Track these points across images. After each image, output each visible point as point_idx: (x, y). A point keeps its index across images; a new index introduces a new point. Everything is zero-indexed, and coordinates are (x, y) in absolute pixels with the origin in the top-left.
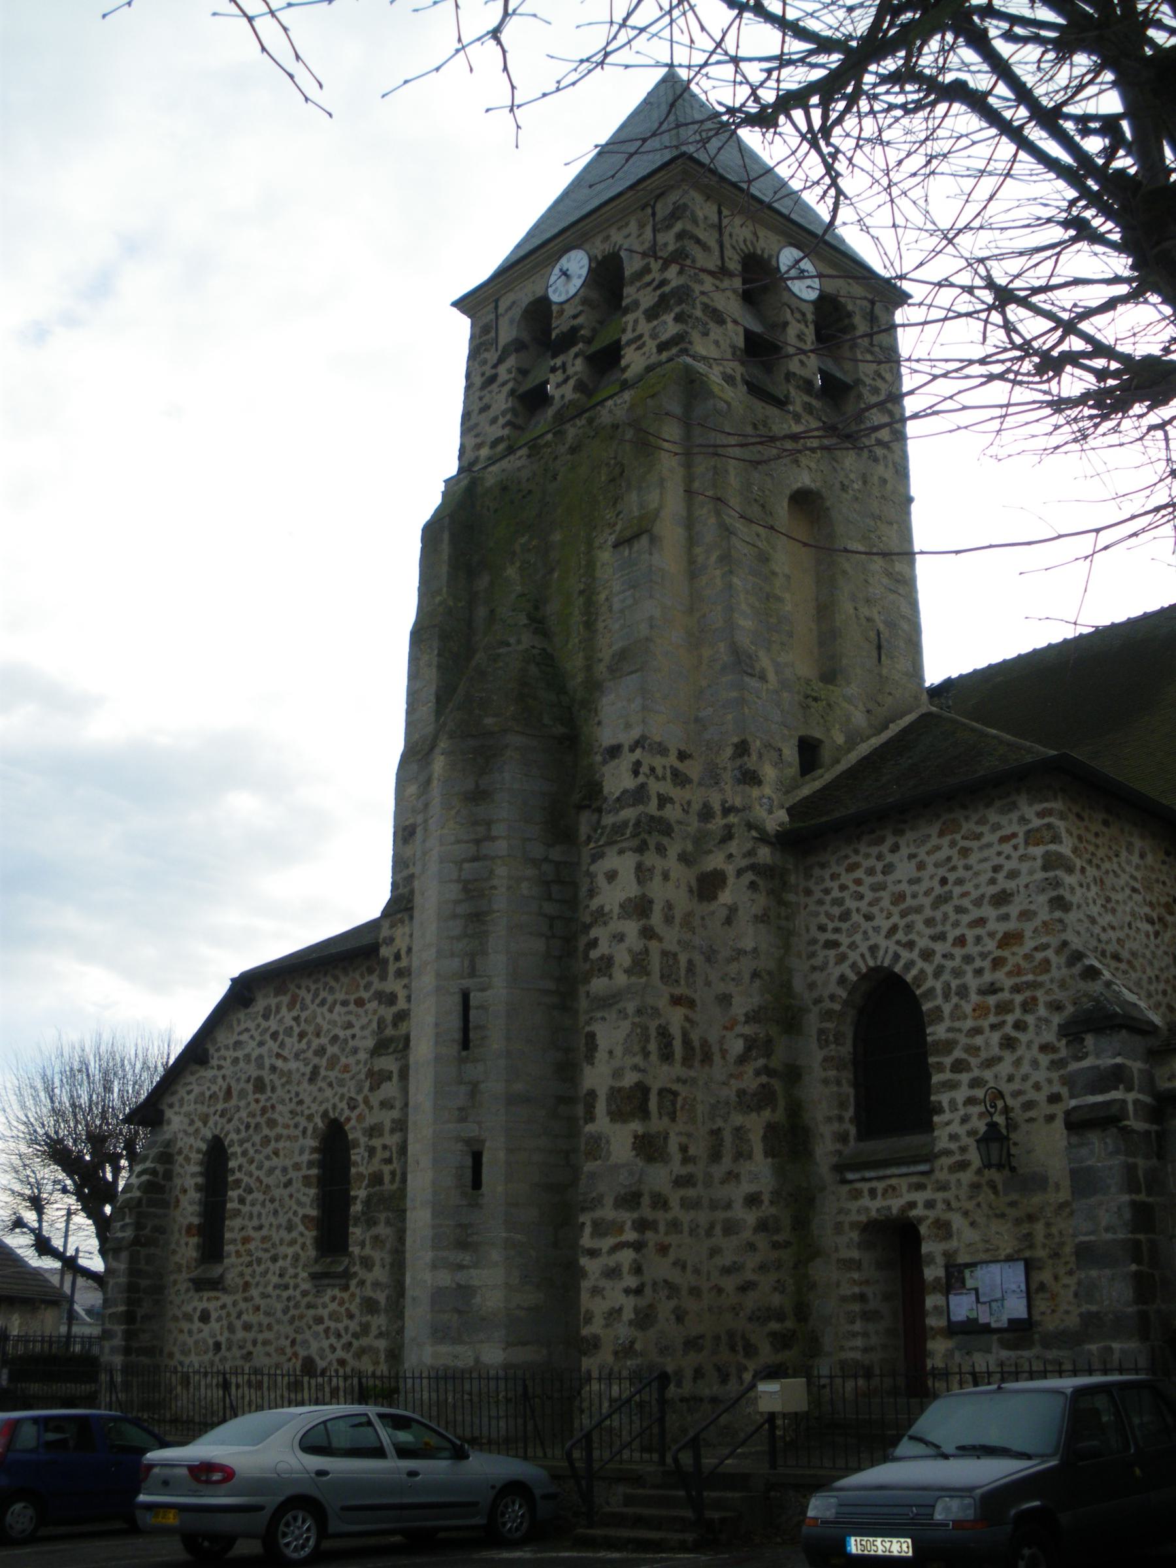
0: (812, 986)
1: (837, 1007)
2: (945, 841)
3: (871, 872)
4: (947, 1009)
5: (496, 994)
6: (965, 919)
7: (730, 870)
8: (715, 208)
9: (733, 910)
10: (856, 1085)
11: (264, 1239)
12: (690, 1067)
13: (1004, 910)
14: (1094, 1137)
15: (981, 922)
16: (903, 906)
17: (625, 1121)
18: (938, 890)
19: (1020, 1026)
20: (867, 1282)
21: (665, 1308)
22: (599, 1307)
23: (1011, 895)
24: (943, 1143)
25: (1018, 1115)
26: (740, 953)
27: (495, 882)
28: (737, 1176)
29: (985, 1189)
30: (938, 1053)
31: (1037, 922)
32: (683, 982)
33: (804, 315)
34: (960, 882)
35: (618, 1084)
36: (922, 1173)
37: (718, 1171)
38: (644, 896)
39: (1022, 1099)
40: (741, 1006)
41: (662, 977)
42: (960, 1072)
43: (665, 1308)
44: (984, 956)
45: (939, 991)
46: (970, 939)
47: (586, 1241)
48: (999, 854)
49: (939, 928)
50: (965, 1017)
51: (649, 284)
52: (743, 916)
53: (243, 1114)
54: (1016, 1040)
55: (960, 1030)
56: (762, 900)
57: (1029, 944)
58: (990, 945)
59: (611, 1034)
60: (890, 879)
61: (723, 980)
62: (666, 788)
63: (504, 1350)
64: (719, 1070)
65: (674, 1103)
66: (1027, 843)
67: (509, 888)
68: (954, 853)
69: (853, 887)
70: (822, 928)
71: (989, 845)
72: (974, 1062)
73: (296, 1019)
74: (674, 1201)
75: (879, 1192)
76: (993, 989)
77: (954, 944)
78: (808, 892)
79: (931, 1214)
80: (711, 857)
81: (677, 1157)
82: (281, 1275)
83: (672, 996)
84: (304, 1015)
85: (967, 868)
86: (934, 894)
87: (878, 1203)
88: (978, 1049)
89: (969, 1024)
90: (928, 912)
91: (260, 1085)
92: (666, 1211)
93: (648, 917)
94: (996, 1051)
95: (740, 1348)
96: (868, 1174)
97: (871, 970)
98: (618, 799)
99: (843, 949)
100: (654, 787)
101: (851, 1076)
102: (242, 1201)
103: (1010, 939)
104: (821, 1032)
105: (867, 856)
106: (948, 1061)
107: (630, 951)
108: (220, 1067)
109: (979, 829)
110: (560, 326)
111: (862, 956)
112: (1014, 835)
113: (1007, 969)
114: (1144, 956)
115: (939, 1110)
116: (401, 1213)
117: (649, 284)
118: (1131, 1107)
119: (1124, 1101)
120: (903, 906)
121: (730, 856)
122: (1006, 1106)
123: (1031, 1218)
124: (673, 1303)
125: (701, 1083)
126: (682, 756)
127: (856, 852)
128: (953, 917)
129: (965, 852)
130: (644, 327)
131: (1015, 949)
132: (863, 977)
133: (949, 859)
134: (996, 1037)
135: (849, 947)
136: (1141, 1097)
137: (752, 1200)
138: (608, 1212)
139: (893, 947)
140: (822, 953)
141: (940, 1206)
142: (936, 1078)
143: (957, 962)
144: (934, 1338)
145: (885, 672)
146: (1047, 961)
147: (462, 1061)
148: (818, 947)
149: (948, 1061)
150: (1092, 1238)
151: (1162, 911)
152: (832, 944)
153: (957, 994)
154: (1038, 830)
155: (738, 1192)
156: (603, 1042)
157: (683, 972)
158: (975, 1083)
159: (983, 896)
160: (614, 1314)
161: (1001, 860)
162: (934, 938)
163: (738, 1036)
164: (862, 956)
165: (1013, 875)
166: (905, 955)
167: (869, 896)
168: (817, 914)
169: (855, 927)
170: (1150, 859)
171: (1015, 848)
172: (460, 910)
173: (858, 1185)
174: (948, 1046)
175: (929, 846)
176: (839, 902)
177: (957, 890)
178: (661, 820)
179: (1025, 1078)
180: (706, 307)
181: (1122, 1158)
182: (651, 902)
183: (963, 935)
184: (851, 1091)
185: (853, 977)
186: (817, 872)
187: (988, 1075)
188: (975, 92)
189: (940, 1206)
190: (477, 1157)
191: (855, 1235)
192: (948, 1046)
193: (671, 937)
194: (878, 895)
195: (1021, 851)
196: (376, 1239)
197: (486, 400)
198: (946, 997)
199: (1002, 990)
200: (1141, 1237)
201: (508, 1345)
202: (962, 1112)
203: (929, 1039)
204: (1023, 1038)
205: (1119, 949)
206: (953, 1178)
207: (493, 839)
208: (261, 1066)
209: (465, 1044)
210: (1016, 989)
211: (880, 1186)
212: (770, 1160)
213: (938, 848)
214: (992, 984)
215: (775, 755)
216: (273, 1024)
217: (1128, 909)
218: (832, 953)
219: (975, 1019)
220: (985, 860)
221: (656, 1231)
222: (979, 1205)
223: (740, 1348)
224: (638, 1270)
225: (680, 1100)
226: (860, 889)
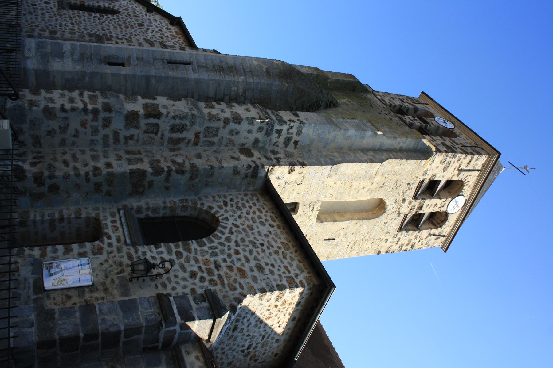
0: (206, 197)
1: (199, 206)
2: (280, 245)
3: (259, 217)
4: (205, 248)
5: (192, 75)
6: (247, 254)
7: (254, 159)
8: (480, 169)
9: (238, 159)
10: (163, 218)
11: (81, 22)
12: (168, 143)
13: (255, 269)
14: (155, 309)
15: (248, 261)
16: (247, 229)
17: (143, 108)
18: (258, 243)
19: (202, 279)
20: (70, 222)
21: (54, 125)
23: (262, 272)
25: (159, 281)
26: (221, 162)
27: (236, 77)
28: (120, 160)
29: (120, 269)
30: (184, 246)
31: (252, 284)
32: (205, 139)
34: (263, 251)
35: (160, 107)
36: (125, 241)
37: (122, 153)
38: (242, 119)
39: (167, 282)
40: (198, 162)
41: (208, 128)
42: (177, 255)
43: (54, 125)
44: (232, 262)
45: (213, 245)
46: (238, 256)
47: (86, 93)
48: (280, 266)
49: (241, 244)
50: (202, 256)
53: (129, 20)
54: (196, 278)
55: (196, 254)
56: (243, 171)
57: (242, 281)
58: (238, 265)
59: (182, 106)
60: (258, 224)
61: (208, 156)
62: (284, 135)
63: (33, 69)
64: (168, 154)
65: (152, 132)
66: (287, 277)
67: (234, 81)
69: (251, 211)
70: (231, 200)
71: (282, 262)
72: (182, 260)
73: (167, 36)
74: (107, 131)
75: (115, 224)
76: (218, 267)
77: (235, 250)
78: (246, 195)
79: (105, 246)
80: (258, 153)
81: (128, 134)
82: (65, 25)
83: (199, 133)
84: (169, 39)
85: (270, 254)
86: (256, 241)
87: (110, 224)
88: (188, 262)
89: (200, 258)
90: (247, 239)
91: (141, 25)
92: (102, 126)
94: (189, 269)
95: (35, 160)
96: (123, 220)
97: (217, 219)
99: (224, 208)
100: (285, 128)
101: (167, 215)
102: (95, 17)
103: (242, 272)
104: (187, 200)
105: (266, 216)
106: (181, 249)
107: (218, 114)
108: (146, 15)
109: (288, 257)
111: (223, 215)
112: (289, 272)
113: (228, 271)
114: (234, 344)
115: (157, 247)
118: (172, 328)
119: (175, 324)
120: (247, 229)
121: (260, 159)
122: (162, 275)
123: (106, 290)
124: (57, 128)
125: (161, 147)
126: (296, 143)
128: (247, 249)
129: (277, 252)
131: (238, 275)
132: (213, 216)
133: (272, 246)
134: (195, 269)
135: (226, 210)
136: (177, 335)
137: (109, 165)
138: (101, 100)
139: (229, 226)
140: (221, 200)
141: (110, 249)
142: (172, 245)
143: (227, 251)
144: (40, 250)
145: (320, 242)
146: (235, 289)
147: (162, 60)
148: (223, 199)
149: (181, 249)
150: (98, 313)
151: (252, 354)
152: (226, 204)
153: (213, 252)
154: (294, 281)
155: (112, 159)
156: (177, 103)
157: (210, 139)
158: (172, 262)
159: (259, 260)
161: (277, 267)
162: (236, 242)
163: (184, 160)
164: (223, 215)
165: (272, 272)
166: (227, 231)
167: (249, 217)
168: (237, 198)
170: (275, 345)
171: (284, 273)
172: (224, 63)
173: (117, 216)
176: (244, 206)
177: (259, 250)
179: (177, 283)
180: (450, 163)
181: (144, 325)
182: (239, 123)
184: (160, 215)
185: (213, 212)
187: (176, 267)
189: (110, 249)
191: (93, 215)
192: (188, 250)
193: (224, 133)
194: (250, 220)
195: (283, 275)
198: (210, 248)
199: (218, 270)
200: (100, 339)
201: (36, 71)
202: (157, 256)
203: (190, 242)
204: (197, 280)
205: (238, 330)
206: (124, 254)
207: (253, 77)
208: (148, 26)
209: (170, 62)
210: (220, 277)
211: (118, 224)
212: (129, 171)
213: (276, 242)
214: (220, 266)
215: (299, 182)
216: (164, 30)
217: (255, 334)
218: (222, 204)
219: (202, 260)
220: (275, 261)
221: (93, 120)
222: (111, 266)
223: (35, 160)
224: (73, 109)
225: (153, 135)
226: (251, 214)
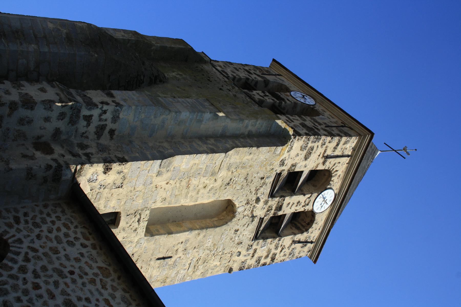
3: (66, 235)
6: (52, 287)
7: (55, 156)
8: (350, 154)
9: (32, 158)
16: (50, 253)
18: (66, 271)
33: (308, 205)
38: (36, 103)
46: (39, 292)
49: (42, 274)
51: (314, 124)
52: (30, 163)
60: (66, 245)
62: (95, 122)
68: (91, 276)
69: (55, 227)
70: (26, 214)
71: (101, 294)
77: (33, 283)
78: (46, 206)
85: (84, 284)
86: (63, 269)
90: (50, 267)
93: (23, 106)
97: (6, 242)
98: (85, 96)
99: (16, 226)
100: (96, 113)
105: (75, 233)
109: (108, 286)
111: (14, 236)
117: (314, 124)
120: (50, 253)
121: (64, 156)
126: (112, 132)
127: (76, 227)
128: (51, 280)
129: (93, 282)
133: (86, 274)
135: (18, 229)
139: (23, 251)
145: (152, 263)
148: (14, 213)
159: (69, 295)
162: (34, 272)
164: (14, 236)
166: (20, 258)
167: (52, 236)
168: (34, 211)
169: (31, 231)
175: (90, 262)
177: (68, 280)
178: (78, 116)
180: (312, 149)
182: (32, 108)
183: (41, 288)
186: (59, 210)
194: (54, 240)
197: (240, 70)
213: (91, 267)
218: (12, 221)
220: (91, 293)
226: (55, 231)
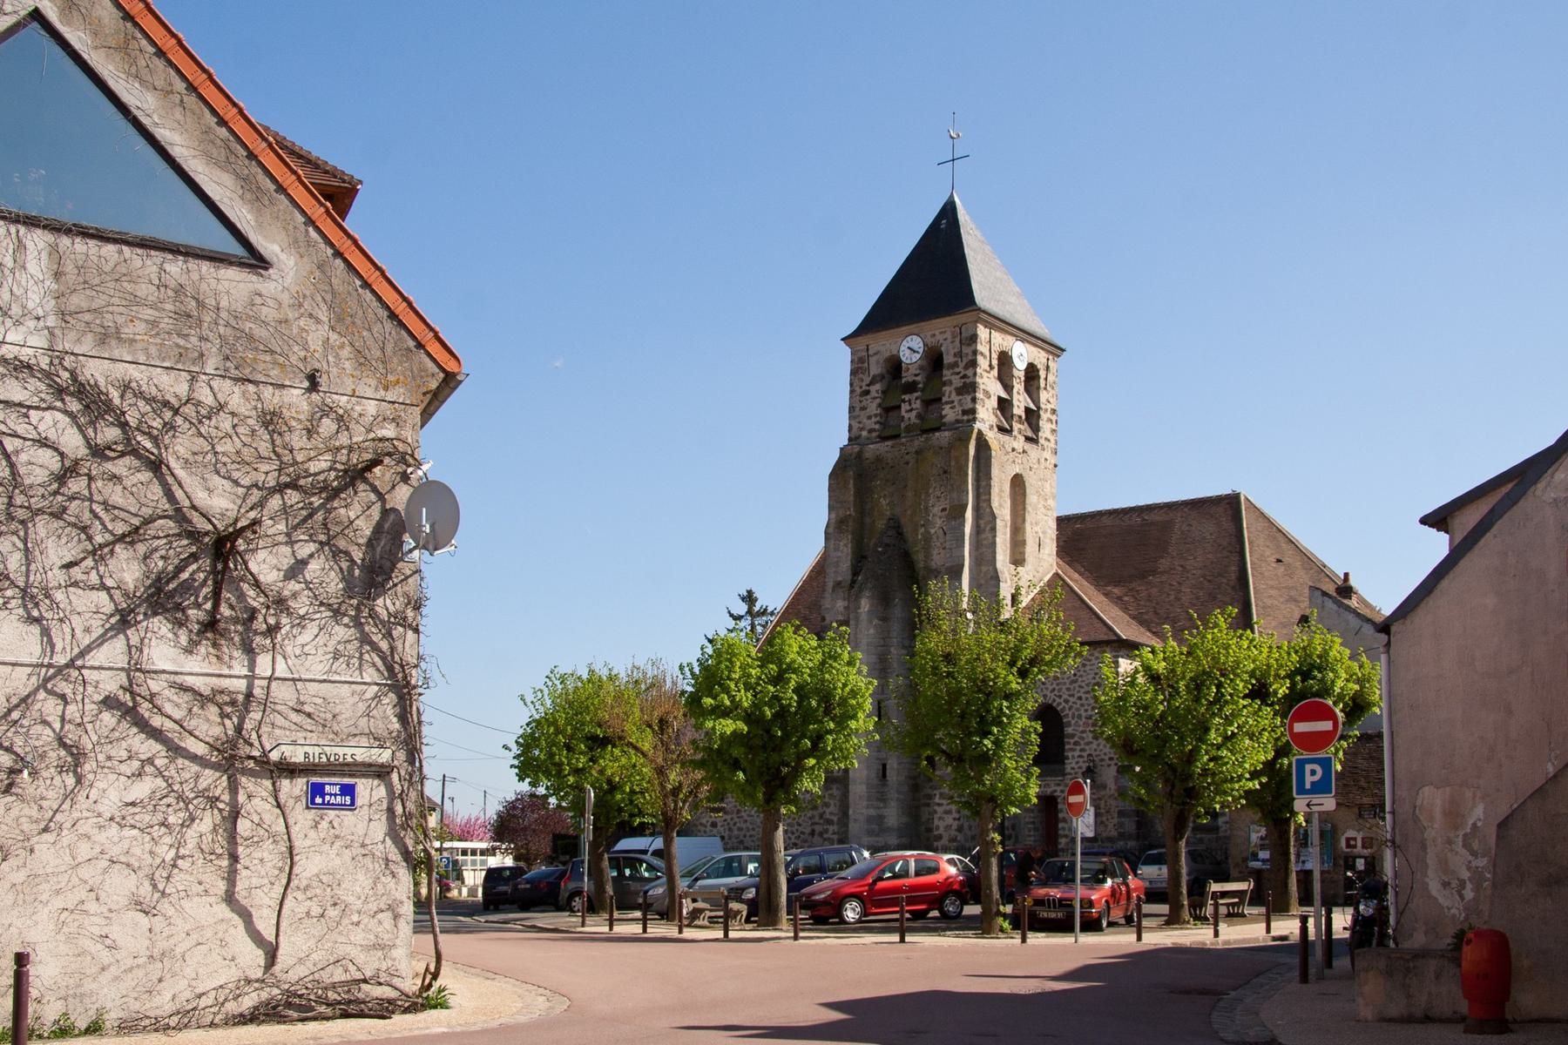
22: (942, 824)
24: (1068, 770)
76: (1090, 717)
110: (907, 377)
116: (846, 786)
130: (954, 396)
160: (948, 827)
174: (1073, 736)
188: (1452, 551)
190: (884, 766)
192: (1073, 736)
196: (831, 796)
